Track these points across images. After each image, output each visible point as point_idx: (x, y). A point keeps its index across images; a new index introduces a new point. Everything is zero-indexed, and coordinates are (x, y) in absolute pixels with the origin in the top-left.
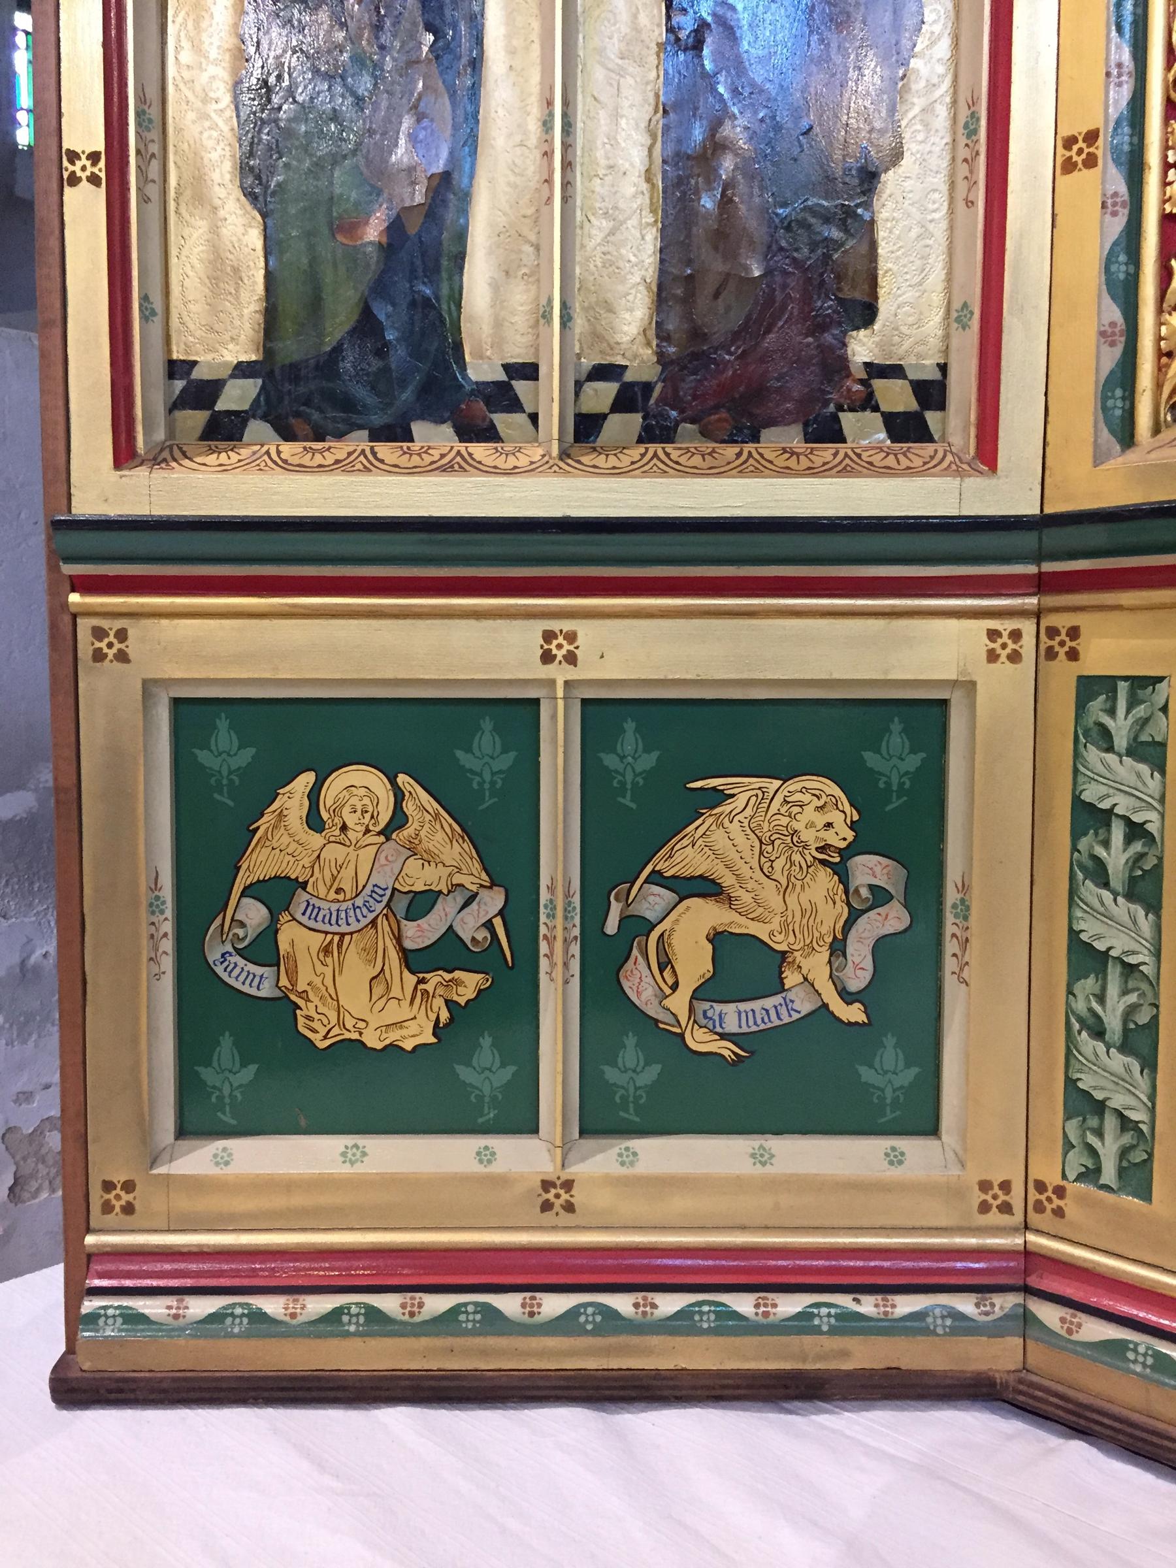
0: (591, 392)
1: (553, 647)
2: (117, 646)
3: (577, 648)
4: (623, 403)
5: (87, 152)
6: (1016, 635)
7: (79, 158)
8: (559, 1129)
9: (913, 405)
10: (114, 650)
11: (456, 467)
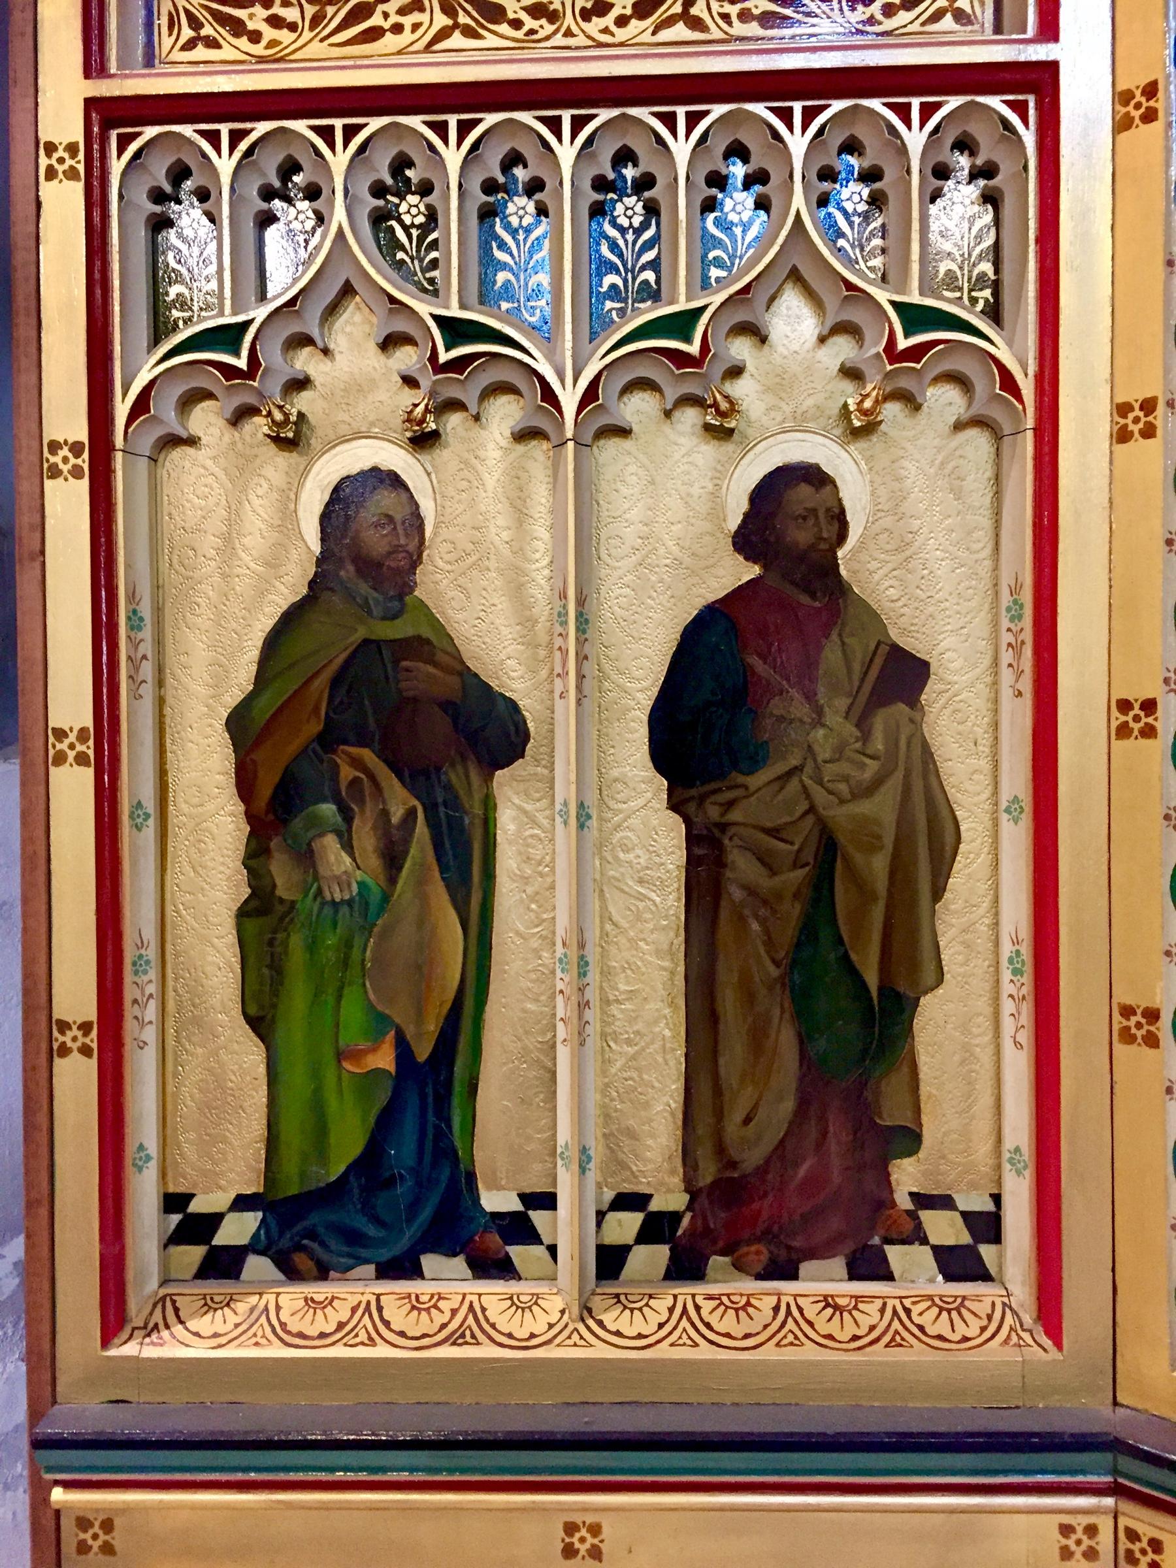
0: (615, 1224)
1: (575, 1540)
2: (103, 1537)
3: (602, 1541)
4: (646, 1236)
5: (79, 1022)
6: (1091, 1530)
7: (70, 1028)
8: (573, 787)
9: (966, 1238)
10: (99, 1542)
11: (468, 1338)
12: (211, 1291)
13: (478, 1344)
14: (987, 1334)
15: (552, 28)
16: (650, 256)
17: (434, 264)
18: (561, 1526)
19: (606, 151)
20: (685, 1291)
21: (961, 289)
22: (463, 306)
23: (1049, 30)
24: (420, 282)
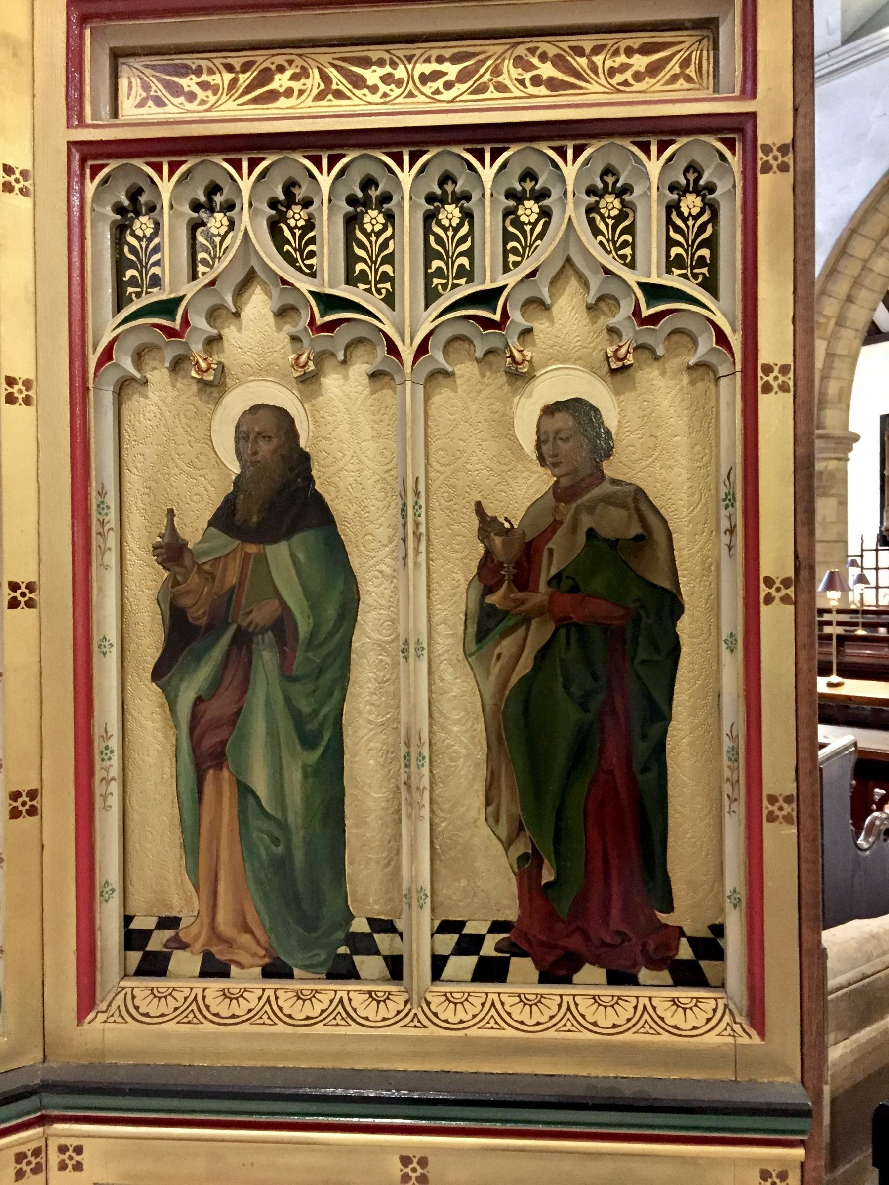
2: (420, 1171)
12: (524, 991)
13: (127, 1022)
14: (133, 1011)
15: (399, 91)
16: (464, 247)
17: (312, 254)
18: (758, 1174)
19: (435, 174)
20: (492, 988)
21: (370, 283)
22: (659, 276)
23: (750, 89)
24: (300, 267)
